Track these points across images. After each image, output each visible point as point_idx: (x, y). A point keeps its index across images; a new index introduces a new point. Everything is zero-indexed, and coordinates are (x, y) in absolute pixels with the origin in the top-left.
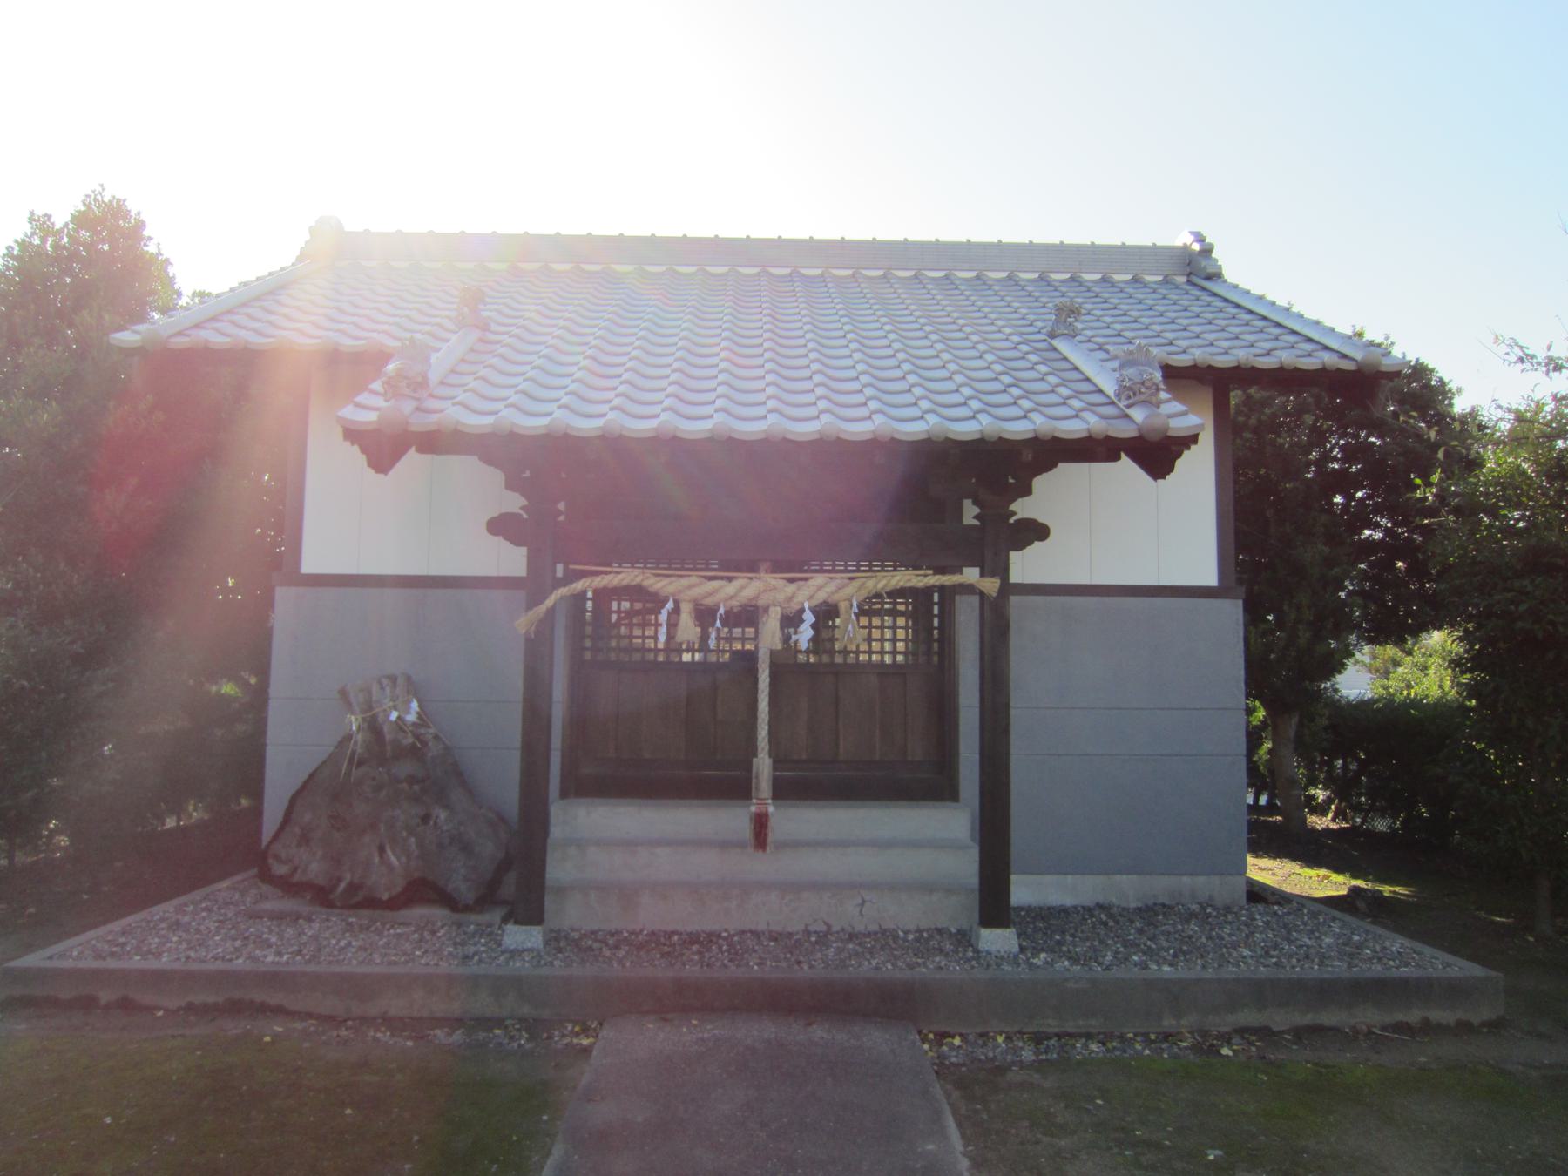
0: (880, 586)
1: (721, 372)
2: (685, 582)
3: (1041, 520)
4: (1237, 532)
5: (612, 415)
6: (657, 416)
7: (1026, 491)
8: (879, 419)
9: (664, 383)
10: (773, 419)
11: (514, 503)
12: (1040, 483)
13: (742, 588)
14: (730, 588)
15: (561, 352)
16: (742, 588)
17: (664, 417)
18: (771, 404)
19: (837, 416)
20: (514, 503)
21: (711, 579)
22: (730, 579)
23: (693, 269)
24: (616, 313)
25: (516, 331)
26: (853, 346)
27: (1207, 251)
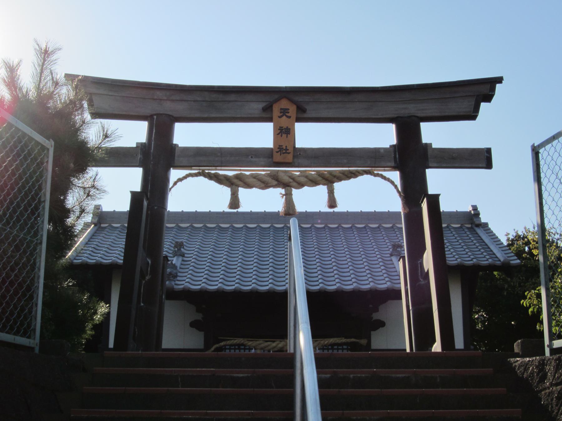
0: (326, 343)
1: (270, 271)
2: (258, 342)
3: (382, 320)
4: (316, 355)
5: (220, 285)
6: (200, 285)
7: (377, 310)
8: (372, 284)
9: (202, 274)
10: (321, 285)
11: (199, 317)
12: (382, 308)
13: (278, 344)
14: (274, 344)
15: (198, 264)
16: (278, 344)
17: (220, 285)
18: (320, 281)
19: (375, 283)
20: (199, 317)
21: (267, 341)
22: (274, 342)
23: (201, 225)
24: (112, 242)
25: (116, 256)
26: (364, 260)
27: (477, 215)
